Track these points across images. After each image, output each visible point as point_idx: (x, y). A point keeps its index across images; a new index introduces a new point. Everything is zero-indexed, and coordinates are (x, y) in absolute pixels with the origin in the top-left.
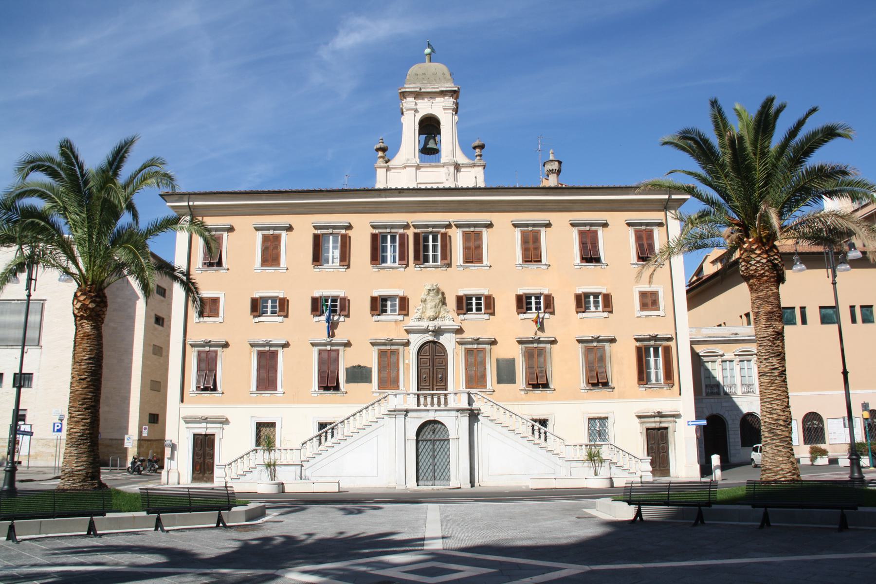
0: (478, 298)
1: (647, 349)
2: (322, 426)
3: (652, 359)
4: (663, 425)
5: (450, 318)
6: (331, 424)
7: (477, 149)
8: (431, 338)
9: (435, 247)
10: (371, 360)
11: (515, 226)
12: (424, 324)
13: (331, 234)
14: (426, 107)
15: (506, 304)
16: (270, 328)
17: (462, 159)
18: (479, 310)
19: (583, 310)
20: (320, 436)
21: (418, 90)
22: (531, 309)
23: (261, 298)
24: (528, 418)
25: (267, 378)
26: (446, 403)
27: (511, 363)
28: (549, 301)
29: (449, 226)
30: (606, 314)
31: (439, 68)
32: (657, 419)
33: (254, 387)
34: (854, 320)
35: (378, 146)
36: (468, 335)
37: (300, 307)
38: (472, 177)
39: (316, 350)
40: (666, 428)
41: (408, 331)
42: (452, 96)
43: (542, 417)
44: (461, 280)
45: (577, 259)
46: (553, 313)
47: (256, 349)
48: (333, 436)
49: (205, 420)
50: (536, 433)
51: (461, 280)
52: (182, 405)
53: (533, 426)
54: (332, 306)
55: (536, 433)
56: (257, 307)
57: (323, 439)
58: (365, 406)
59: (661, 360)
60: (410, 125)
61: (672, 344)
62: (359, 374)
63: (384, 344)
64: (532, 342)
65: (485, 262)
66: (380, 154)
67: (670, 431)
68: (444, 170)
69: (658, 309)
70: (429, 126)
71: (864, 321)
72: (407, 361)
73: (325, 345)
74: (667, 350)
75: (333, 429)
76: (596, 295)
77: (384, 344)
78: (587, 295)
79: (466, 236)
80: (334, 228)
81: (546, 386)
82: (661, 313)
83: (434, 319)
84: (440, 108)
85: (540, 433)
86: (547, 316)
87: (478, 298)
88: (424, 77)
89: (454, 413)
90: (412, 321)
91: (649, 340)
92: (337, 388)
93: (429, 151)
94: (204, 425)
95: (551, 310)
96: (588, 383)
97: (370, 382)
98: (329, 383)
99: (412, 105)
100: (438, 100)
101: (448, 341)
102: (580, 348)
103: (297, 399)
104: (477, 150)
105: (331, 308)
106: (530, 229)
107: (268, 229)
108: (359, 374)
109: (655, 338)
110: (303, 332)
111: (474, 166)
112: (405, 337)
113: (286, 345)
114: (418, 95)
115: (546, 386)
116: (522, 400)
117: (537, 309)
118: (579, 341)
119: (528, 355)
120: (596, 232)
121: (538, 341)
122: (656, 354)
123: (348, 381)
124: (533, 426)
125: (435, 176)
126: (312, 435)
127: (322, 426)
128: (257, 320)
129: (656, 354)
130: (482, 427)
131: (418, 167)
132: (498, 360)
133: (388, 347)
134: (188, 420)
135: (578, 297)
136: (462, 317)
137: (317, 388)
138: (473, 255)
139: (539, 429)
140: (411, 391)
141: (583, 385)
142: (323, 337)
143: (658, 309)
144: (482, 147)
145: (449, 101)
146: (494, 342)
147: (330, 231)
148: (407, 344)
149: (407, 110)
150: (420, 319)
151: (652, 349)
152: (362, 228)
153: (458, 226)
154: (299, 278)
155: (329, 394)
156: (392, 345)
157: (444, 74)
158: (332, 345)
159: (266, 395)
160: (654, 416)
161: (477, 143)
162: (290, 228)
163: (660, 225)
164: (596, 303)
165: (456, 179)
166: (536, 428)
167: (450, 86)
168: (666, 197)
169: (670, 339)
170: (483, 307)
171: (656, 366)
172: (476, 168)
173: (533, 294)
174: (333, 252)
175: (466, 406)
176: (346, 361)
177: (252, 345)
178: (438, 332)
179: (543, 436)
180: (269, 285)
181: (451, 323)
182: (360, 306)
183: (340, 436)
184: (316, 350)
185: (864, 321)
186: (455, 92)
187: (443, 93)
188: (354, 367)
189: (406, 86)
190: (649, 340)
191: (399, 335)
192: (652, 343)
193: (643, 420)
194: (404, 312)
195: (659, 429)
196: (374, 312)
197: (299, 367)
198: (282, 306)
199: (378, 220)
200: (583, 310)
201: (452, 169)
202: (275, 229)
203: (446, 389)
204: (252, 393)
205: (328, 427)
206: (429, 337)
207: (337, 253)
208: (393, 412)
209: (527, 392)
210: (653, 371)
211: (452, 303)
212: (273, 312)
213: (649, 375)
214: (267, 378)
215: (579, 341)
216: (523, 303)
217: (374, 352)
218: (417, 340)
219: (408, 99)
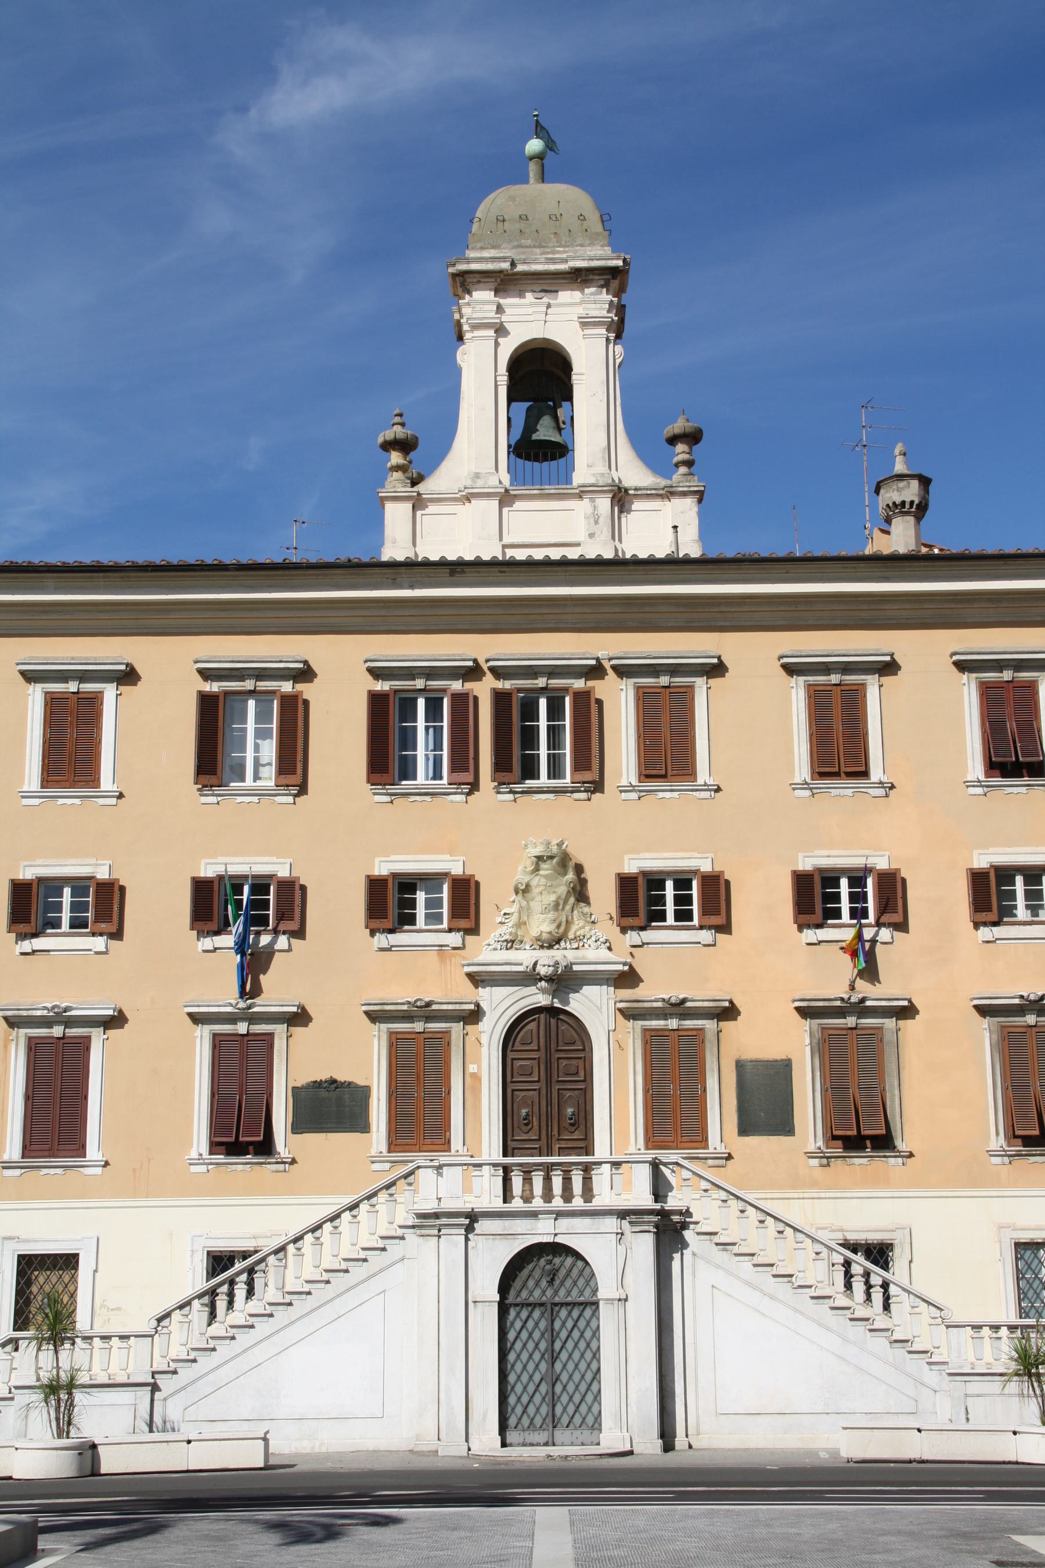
0: (683, 883)
2: (219, 1262)
6: (245, 1255)
7: (676, 443)
9: (555, 733)
10: (369, 1064)
11: (791, 670)
12: (524, 958)
13: (252, 693)
15: (762, 900)
17: (633, 473)
18: (683, 915)
19: (993, 916)
20: (213, 1293)
21: (505, 266)
22: (837, 914)
23: (40, 880)
24: (832, 1238)
27: (782, 1070)
28: (892, 890)
29: (596, 671)
31: (567, 198)
33: (13, 1150)
36: (653, 990)
37: (158, 907)
38: (665, 527)
39: (203, 1036)
41: (477, 980)
42: (606, 285)
43: (874, 1237)
44: (630, 829)
45: (976, 768)
46: (902, 926)
48: (250, 1293)
50: (859, 1286)
51: (630, 829)
53: (847, 1264)
54: (254, 904)
55: (859, 1286)
57: (221, 1304)
58: (347, 1200)
60: (481, 376)
62: (330, 1107)
65: (703, 776)
66: (396, 458)
68: (582, 506)
70: (539, 377)
72: (472, 1068)
75: (251, 1271)
78: (1005, 874)
79: (645, 700)
81: (884, 1143)
83: (553, 942)
84: (570, 321)
85: (869, 1286)
86: (885, 934)
88: (522, 227)
90: (487, 951)
92: (265, 1148)
93: (538, 454)
95: (897, 918)
97: (364, 1127)
98: (241, 1133)
99: (488, 313)
100: (565, 296)
101: (593, 1008)
102: (984, 1030)
103: (141, 1182)
104: (681, 447)
105: (247, 911)
107: (63, 676)
108: (330, 1107)
110: (161, 986)
111: (669, 494)
112: (466, 995)
113: (116, 1021)
114: (507, 282)
115: (884, 1143)
116: (814, 1184)
117: (854, 913)
118: (983, 1011)
119: (832, 1051)
124: (847, 1264)
125: (557, 526)
126: (188, 1292)
127: (219, 1262)
128: (27, 946)
130: (697, 1269)
132: (740, 1065)
133: (418, 1026)
135: (978, 880)
136: (633, 937)
137: (204, 1148)
138: (667, 755)
139: (867, 1274)
140: (484, 1157)
141: (997, 1141)
144: (693, 437)
145: (597, 302)
146: (728, 1012)
147: (249, 685)
148: (474, 1016)
149: (475, 327)
150: (511, 943)
152: (341, 676)
153: (622, 672)
155: (242, 1167)
156: (430, 1018)
157: (582, 218)
159: (52, 1173)
161: (679, 426)
162: (128, 676)
165: (616, 533)
166: (856, 1269)
167: (598, 254)
170: (695, 907)
173: (669, 874)
174: (257, 748)
175: (647, 1201)
176: (296, 1064)
178: (565, 981)
179: (877, 1296)
180: (846, 833)
181: (603, 954)
183: (272, 1294)
187: (579, 277)
188: (317, 1085)
189: (471, 254)
191: (449, 989)
194: (463, 923)
196: (376, 924)
197: (152, 1085)
198: (103, 906)
200: (993, 916)
202: (83, 676)
203: (589, 1150)
204: (8, 1166)
205: (238, 1266)
206: (537, 997)
207: (269, 750)
208: (431, 1221)
209: (827, 1160)
211: (604, 896)
212: (78, 924)
215: (983, 1011)
216: (814, 896)
217: (375, 1044)
218: (502, 1006)
219: (478, 295)
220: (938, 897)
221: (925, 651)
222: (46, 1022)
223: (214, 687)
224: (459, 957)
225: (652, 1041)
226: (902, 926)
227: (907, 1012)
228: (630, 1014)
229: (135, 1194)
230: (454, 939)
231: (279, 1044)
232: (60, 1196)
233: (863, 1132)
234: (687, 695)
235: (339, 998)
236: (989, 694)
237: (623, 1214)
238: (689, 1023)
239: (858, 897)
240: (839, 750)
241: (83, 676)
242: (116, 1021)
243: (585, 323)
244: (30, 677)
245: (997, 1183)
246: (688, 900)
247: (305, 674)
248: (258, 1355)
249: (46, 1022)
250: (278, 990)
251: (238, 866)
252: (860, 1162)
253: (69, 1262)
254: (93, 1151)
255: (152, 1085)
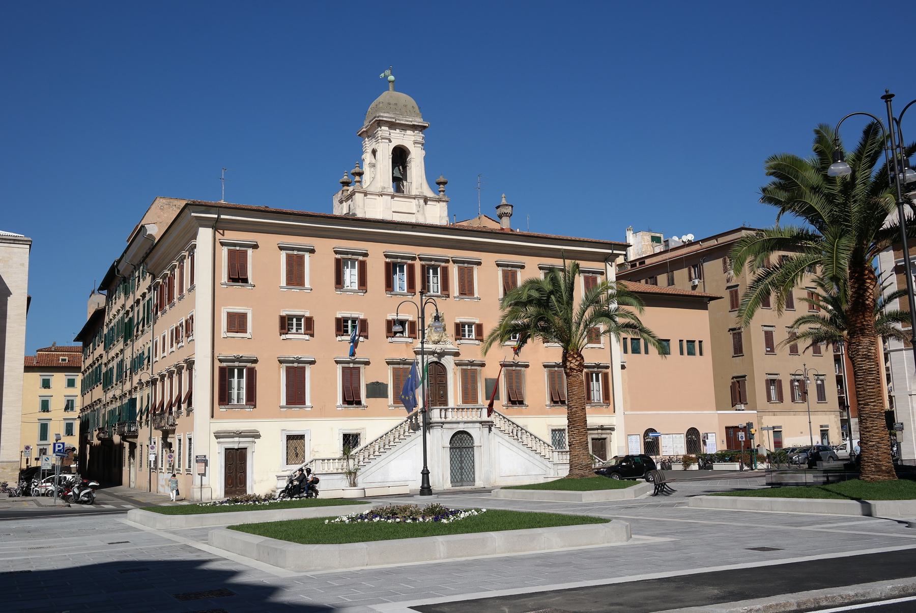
0: (354, 321)
1: (231, 370)
3: (235, 380)
4: (604, 436)
5: (450, 344)
7: (438, 184)
8: (436, 359)
10: (387, 377)
11: (498, 265)
14: (408, 139)
16: (297, 345)
17: (429, 194)
22: (347, 331)
25: (296, 396)
26: (446, 418)
30: (307, 337)
31: (404, 98)
32: (600, 431)
33: (283, 402)
34: (682, 353)
35: (353, 171)
36: (465, 357)
37: (325, 326)
38: (436, 214)
39: (339, 367)
40: (605, 439)
44: (456, 310)
46: (366, 337)
47: (285, 365)
49: (239, 434)
51: (456, 310)
52: (213, 420)
56: (285, 324)
59: (244, 381)
61: (609, 371)
62: (377, 390)
63: (399, 363)
64: (511, 366)
65: (476, 296)
67: (608, 440)
69: (244, 331)
70: (400, 156)
71: (689, 354)
73: (348, 362)
74: (606, 376)
76: (299, 318)
77: (399, 363)
78: (290, 318)
79: (461, 270)
80: (353, 254)
81: (521, 403)
82: (601, 346)
84: (408, 139)
86: (361, 339)
87: (354, 321)
88: (392, 107)
89: (478, 425)
91: (594, 367)
92: (359, 403)
93: (399, 181)
94: (236, 439)
96: (510, 400)
97: (387, 397)
98: (351, 399)
99: (386, 134)
100: (409, 132)
101: (448, 362)
102: (545, 372)
103: (322, 412)
106: (509, 269)
107: (293, 249)
108: (377, 390)
109: (239, 359)
110: (325, 353)
111: (439, 201)
113: (312, 363)
114: (392, 125)
115: (521, 403)
118: (545, 366)
119: (509, 376)
120: (302, 257)
121: (517, 365)
122: (240, 376)
123: (368, 396)
129: (240, 376)
131: (393, 197)
133: (401, 366)
134: (218, 436)
135: (282, 319)
138: (467, 289)
142: (346, 357)
143: (244, 331)
144: (444, 183)
145: (419, 136)
146: (483, 365)
147: (350, 256)
149: (383, 138)
151: (236, 371)
152: (377, 255)
153: (455, 262)
154: (320, 298)
155: (352, 409)
156: (404, 364)
158: (354, 362)
159: (296, 410)
160: (597, 429)
161: (442, 179)
162: (255, 247)
163: (602, 273)
164: (299, 325)
167: (418, 121)
168: (610, 251)
169: (607, 367)
171: (238, 386)
172: (441, 203)
174: (351, 276)
176: (366, 377)
177: (281, 362)
178: (442, 354)
180: (296, 304)
182: (377, 328)
184: (339, 367)
185: (689, 354)
186: (425, 127)
187: (414, 127)
188: (373, 383)
190: (594, 367)
191: (410, 356)
192: (236, 364)
193: (221, 440)
195: (599, 439)
197: (326, 382)
199: (391, 250)
201: (422, 201)
202: (299, 250)
203: (447, 405)
204: (282, 407)
207: (356, 279)
209: (507, 407)
210: (235, 392)
211: (451, 330)
213: (230, 395)
214: (296, 396)
215: (545, 366)
216: (341, 326)
217: (389, 370)
219: (383, 128)
220: (377, 328)
221: (489, 259)
222: (293, 362)
223: (338, 256)
224: (411, 346)
225: (464, 372)
226: (366, 337)
227: (527, 366)
228: (457, 365)
229: (321, 416)
230: (410, 340)
231: (362, 371)
232: (251, 418)
233: (516, 401)
234: (471, 270)
235: (380, 356)
236: (289, 258)
237: (481, 423)
238: (301, 365)
239: (299, 325)
240: (295, 276)
241: (299, 250)
242: (312, 363)
243: (415, 143)
244: (281, 248)
245: (548, 414)
246: (300, 325)
247: (366, 255)
248: (383, 463)
249: (293, 362)
250: (360, 355)
251: (347, 314)
252: (516, 408)
253: (302, 437)
254: (308, 403)
255: (326, 382)
